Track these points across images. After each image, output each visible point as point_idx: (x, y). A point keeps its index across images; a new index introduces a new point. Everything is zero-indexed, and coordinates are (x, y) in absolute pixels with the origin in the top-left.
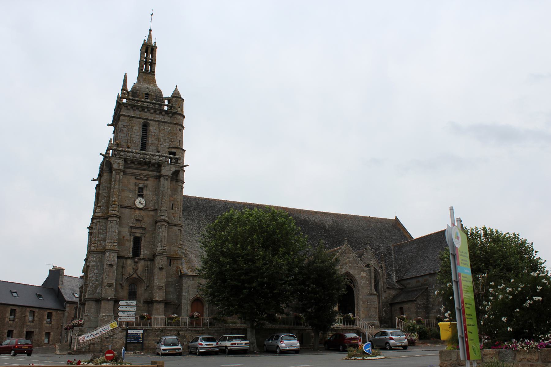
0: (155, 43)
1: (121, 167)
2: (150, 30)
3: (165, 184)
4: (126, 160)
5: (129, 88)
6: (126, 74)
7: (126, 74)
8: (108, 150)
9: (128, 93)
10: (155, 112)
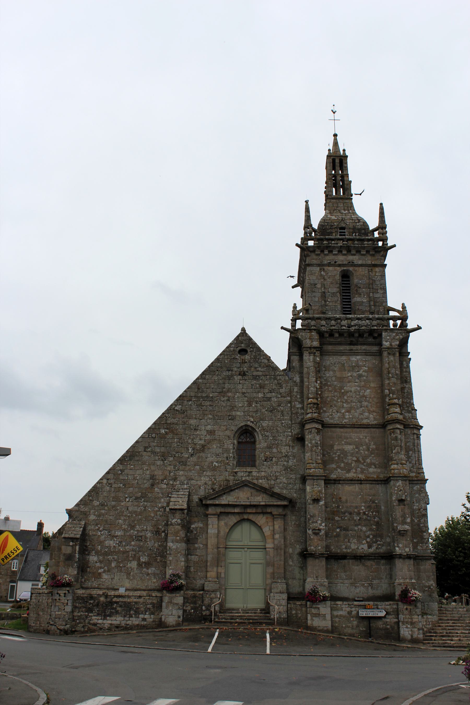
0: (344, 150)
1: (316, 344)
2: (335, 135)
3: (390, 360)
4: (321, 334)
5: (315, 225)
6: (381, 204)
7: (381, 204)
8: (294, 320)
9: (314, 230)
10: (368, 252)
